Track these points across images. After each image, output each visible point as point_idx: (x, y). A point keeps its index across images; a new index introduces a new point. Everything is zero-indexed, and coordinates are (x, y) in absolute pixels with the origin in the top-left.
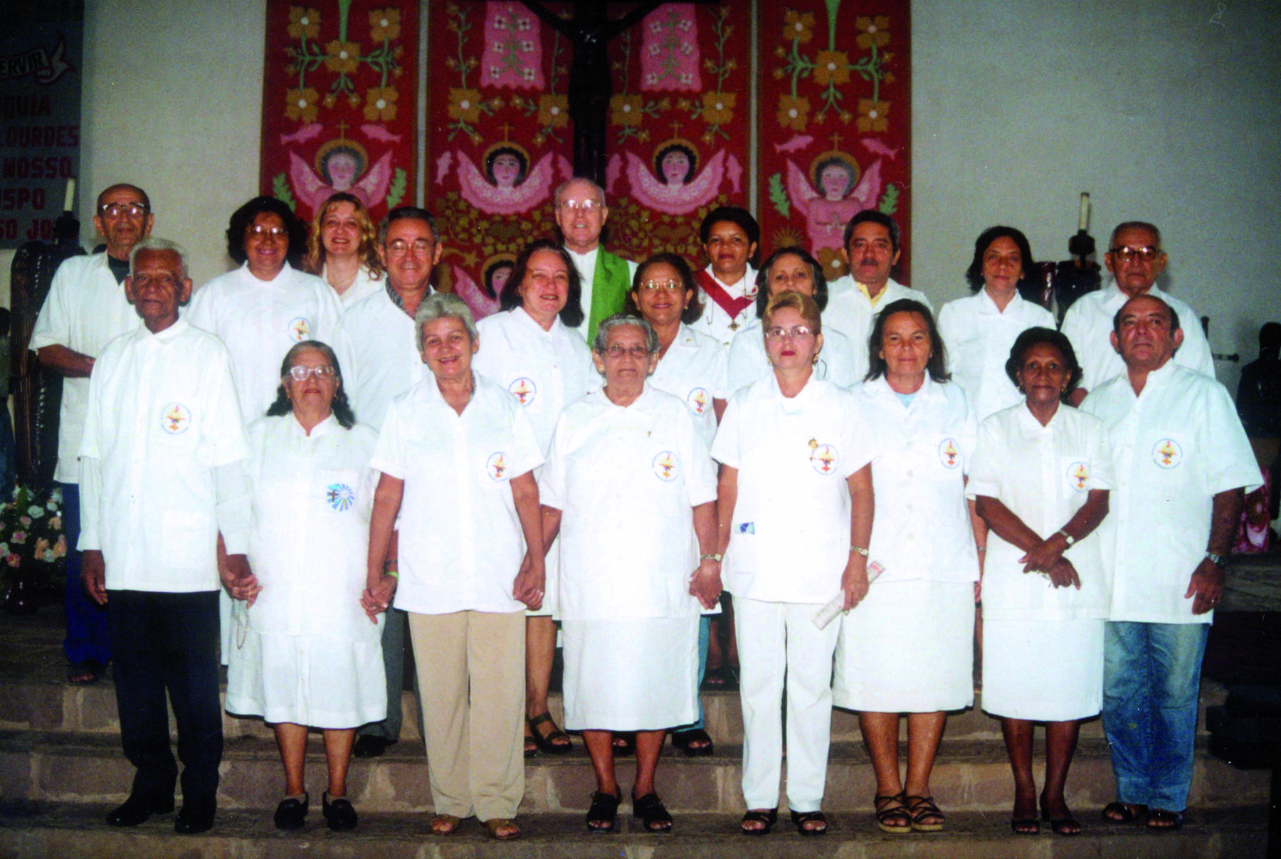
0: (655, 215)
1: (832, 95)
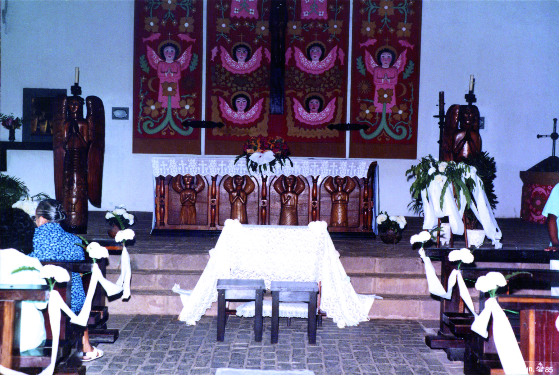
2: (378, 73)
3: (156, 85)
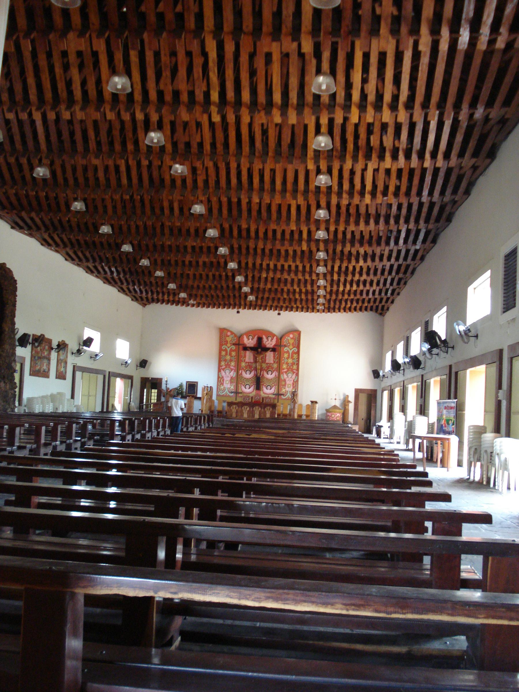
0: (267, 379)
1: (290, 364)
2: (287, 380)
3: (223, 380)
